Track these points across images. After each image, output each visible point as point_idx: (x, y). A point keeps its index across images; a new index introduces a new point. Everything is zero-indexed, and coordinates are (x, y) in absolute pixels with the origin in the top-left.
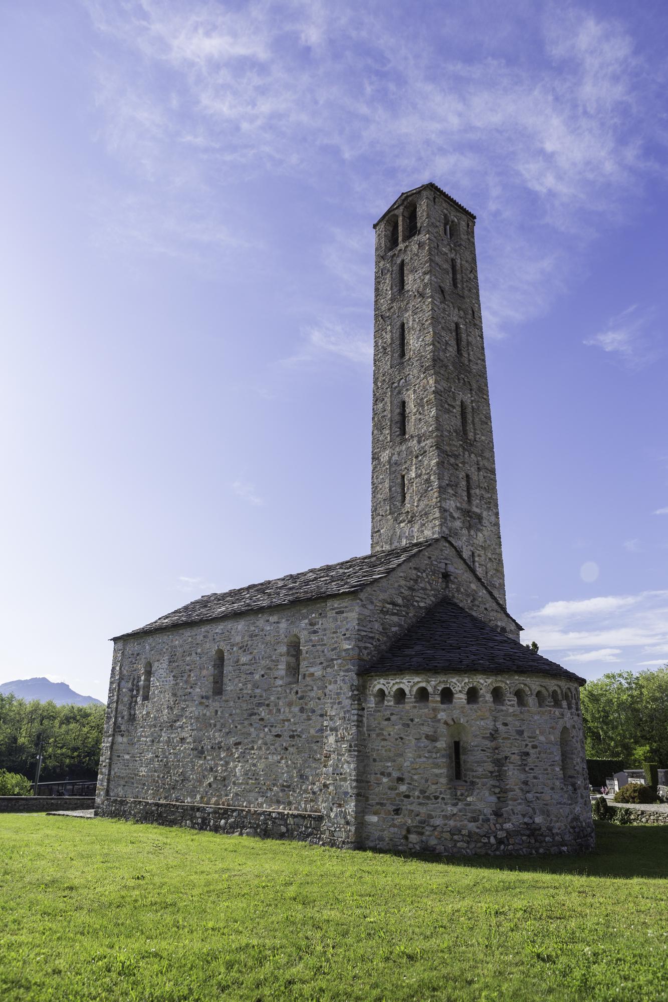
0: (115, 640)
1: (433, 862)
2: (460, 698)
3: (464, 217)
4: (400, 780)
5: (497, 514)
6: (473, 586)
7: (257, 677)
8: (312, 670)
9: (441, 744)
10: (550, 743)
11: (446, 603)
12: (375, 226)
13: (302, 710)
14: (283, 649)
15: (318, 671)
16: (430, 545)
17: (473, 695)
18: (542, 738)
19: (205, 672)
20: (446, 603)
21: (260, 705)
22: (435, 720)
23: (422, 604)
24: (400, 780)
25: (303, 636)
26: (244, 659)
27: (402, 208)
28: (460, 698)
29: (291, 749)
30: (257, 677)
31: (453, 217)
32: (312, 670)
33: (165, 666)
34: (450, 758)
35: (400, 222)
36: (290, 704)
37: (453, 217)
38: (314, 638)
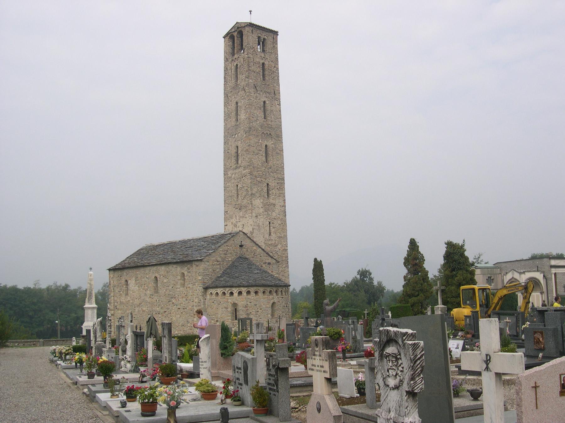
0: (110, 270)
1: (28, 291)
2: (236, 294)
3: (271, 34)
4: (217, 321)
5: (285, 200)
6: (254, 248)
7: (170, 287)
8: (189, 286)
9: (229, 310)
10: (267, 307)
11: (242, 258)
12: (224, 37)
13: (186, 300)
14: (179, 277)
15: (191, 286)
16: (233, 236)
17: (240, 293)
18: (264, 306)
19: (150, 285)
20: (242, 258)
21: (172, 298)
22: (227, 302)
23: (230, 259)
24: (217, 321)
25: (186, 273)
26: (165, 281)
27: (236, 32)
28: (236, 294)
29: (184, 313)
30: (170, 287)
31: (263, 35)
32: (189, 286)
33: (134, 282)
34: (233, 313)
35: (237, 37)
36: (183, 298)
37: (263, 35)
38: (190, 274)
